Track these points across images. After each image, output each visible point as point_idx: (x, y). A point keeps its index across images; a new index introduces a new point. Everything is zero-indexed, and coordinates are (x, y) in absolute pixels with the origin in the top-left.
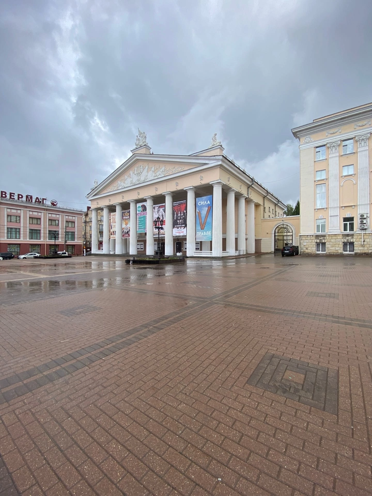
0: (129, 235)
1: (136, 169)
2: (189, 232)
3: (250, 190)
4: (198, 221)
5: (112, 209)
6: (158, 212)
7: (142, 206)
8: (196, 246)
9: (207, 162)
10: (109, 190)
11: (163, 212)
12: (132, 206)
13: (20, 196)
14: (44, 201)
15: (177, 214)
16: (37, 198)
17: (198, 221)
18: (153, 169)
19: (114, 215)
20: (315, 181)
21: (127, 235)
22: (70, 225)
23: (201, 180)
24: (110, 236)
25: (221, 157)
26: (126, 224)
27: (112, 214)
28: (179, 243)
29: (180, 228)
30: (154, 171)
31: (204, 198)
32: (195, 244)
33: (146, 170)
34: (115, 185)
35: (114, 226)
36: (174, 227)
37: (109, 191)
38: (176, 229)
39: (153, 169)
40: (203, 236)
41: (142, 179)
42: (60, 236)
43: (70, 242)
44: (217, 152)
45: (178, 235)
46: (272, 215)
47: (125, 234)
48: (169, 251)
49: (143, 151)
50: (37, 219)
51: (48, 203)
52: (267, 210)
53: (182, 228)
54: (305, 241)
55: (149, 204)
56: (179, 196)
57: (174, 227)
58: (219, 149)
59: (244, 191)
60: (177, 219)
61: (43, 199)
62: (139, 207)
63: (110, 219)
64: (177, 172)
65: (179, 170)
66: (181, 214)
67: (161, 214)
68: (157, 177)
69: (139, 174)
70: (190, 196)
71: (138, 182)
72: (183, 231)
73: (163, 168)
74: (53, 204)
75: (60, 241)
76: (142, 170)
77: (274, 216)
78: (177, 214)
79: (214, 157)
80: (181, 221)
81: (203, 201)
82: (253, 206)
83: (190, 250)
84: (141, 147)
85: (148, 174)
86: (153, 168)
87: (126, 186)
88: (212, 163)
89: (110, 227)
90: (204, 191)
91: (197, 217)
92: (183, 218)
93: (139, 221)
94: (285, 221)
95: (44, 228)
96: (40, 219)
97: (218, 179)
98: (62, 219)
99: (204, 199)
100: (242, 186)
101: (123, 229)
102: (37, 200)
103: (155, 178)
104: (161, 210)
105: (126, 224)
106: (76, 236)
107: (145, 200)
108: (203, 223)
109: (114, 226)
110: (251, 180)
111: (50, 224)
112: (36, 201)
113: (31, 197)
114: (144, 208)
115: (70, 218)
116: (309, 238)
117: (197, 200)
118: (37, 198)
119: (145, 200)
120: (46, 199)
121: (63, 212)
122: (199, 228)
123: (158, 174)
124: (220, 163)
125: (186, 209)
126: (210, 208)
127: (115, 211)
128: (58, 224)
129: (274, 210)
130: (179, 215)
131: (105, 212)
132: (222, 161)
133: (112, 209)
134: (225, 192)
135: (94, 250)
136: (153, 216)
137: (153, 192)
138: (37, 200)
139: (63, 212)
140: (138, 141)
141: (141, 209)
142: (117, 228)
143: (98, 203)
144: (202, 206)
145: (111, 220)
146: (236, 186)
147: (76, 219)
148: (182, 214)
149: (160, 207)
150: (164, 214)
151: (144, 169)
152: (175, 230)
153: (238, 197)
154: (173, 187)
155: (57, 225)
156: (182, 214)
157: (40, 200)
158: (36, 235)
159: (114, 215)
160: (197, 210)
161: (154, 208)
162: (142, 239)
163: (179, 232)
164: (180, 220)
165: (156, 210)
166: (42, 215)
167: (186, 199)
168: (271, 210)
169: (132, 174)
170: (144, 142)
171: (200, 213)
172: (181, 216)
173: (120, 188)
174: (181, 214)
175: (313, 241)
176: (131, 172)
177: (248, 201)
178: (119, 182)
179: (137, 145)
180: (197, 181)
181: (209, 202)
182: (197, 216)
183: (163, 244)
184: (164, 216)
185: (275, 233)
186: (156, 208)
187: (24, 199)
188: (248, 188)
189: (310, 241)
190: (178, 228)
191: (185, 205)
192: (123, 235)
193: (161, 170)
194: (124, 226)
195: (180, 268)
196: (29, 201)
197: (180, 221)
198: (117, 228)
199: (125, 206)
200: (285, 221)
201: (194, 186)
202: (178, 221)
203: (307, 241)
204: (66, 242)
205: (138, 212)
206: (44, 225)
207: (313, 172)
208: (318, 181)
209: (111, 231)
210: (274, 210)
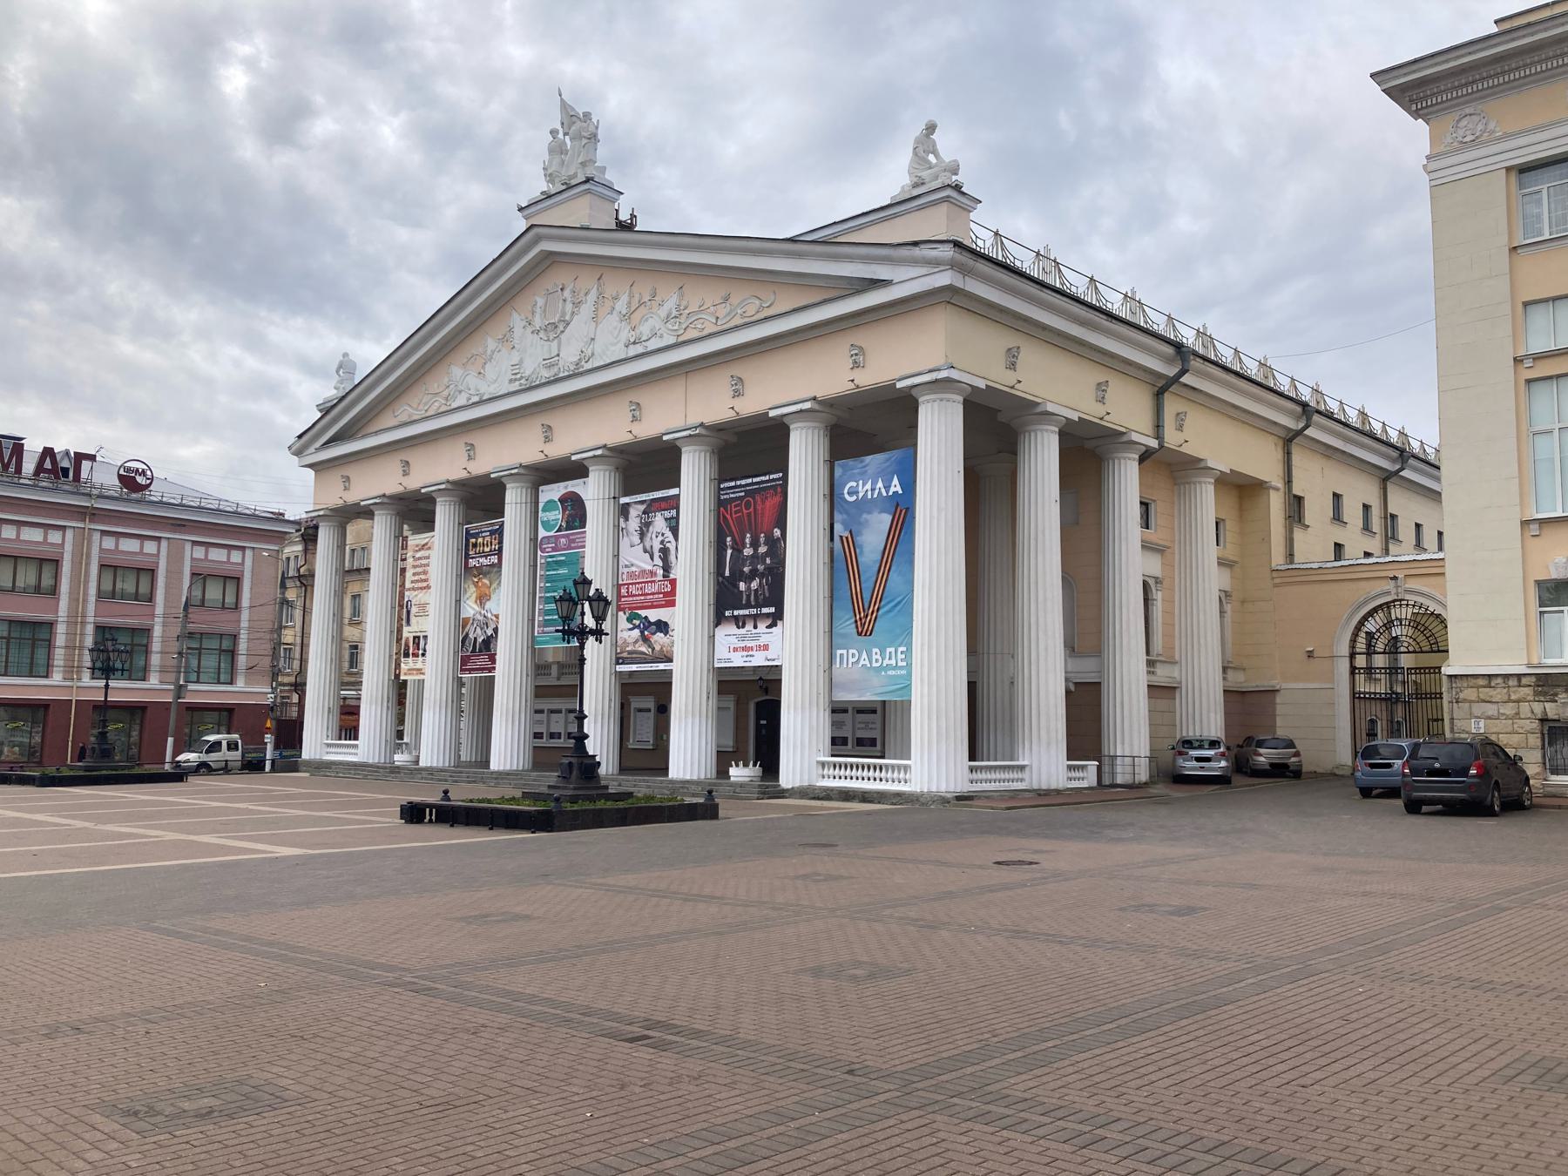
0: (493, 659)
1: (540, 301)
2: (790, 646)
3: (1171, 406)
4: (843, 592)
5: (414, 511)
6: (642, 535)
7: (563, 500)
8: (835, 724)
9: (881, 272)
10: (404, 411)
11: (669, 534)
12: (514, 498)
14: (86, 465)
15: (738, 549)
17: (843, 592)
18: (621, 305)
19: (423, 547)
20: (1518, 361)
21: (483, 660)
22: (214, 592)
23: (856, 365)
24: (398, 666)
25: (947, 252)
26: (482, 599)
27: (415, 540)
28: (752, 705)
29: (749, 626)
30: (626, 317)
31: (874, 461)
32: (828, 713)
33: (587, 309)
34: (434, 387)
35: (423, 606)
36: (719, 619)
37: (404, 418)
38: (732, 629)
39: (621, 305)
40: (865, 670)
41: (569, 356)
42: (155, 660)
43: (203, 692)
44: (933, 224)
45: (738, 661)
46: (1356, 544)
47: (476, 651)
48: (689, 752)
49: (577, 212)
50: (42, 561)
52: (1317, 510)
53: (762, 626)
54: (1478, 709)
55: (595, 490)
56: (751, 449)
57: (719, 619)
58: (944, 207)
59: (1127, 411)
60: (737, 575)
61: (80, 457)
62: (550, 505)
63: (403, 570)
64: (738, 321)
65: (751, 309)
66: (755, 544)
67: (657, 547)
68: (639, 349)
69: (555, 329)
70: (804, 454)
71: (546, 374)
72: (763, 640)
73: (671, 304)
75: (153, 687)
76: (569, 307)
77: (1374, 545)
78: (738, 549)
79: (917, 252)
80: (754, 585)
81: (867, 482)
82: (1206, 502)
83: (803, 751)
84: (571, 187)
85: (599, 330)
86: (624, 298)
87: (488, 390)
88: (908, 281)
89: (402, 611)
90: (870, 427)
91: (840, 564)
92: (769, 569)
93: (548, 579)
94: (1412, 584)
95: (74, 612)
97: (939, 361)
98: (174, 564)
99: (871, 470)
101: (466, 621)
102: (48, 465)
103: (633, 351)
104: (659, 522)
105: (482, 599)
106: (242, 661)
107: (577, 470)
108: (865, 597)
109: (423, 606)
110: (1170, 350)
111: (107, 586)
112: (39, 469)
114: (575, 511)
115: (217, 555)
116: (1498, 694)
117: (838, 472)
118: (48, 452)
119: (577, 470)
120: (92, 458)
121: (180, 525)
122: (847, 626)
123: (645, 330)
124: (944, 279)
125: (783, 526)
126: (902, 512)
127: (425, 522)
129: (1376, 513)
130: (748, 551)
131: (380, 530)
132: (953, 265)
133: (414, 511)
134: (994, 429)
135: (316, 741)
136: (617, 556)
137: (612, 427)
138: (48, 465)
139: (180, 525)
140: (557, 160)
141: (557, 516)
142: (432, 622)
144: (864, 505)
145: (409, 574)
146: (1061, 388)
147: (245, 561)
148: (763, 549)
149: (652, 507)
150: (672, 546)
151: (577, 304)
152: (727, 636)
153: (1086, 453)
154: (713, 403)
156: (763, 549)
157: (65, 464)
158: (27, 651)
159: (423, 547)
160: (838, 528)
161: (624, 511)
162: (556, 686)
163: (738, 648)
164: (754, 574)
165: (634, 524)
166: (64, 541)
167: (784, 469)
168: (1352, 513)
169: (518, 331)
170: (583, 164)
171: (851, 543)
172: (755, 556)
173: (461, 401)
174: (755, 544)
175: (1525, 707)
176: (517, 320)
177: (1170, 468)
178: (456, 371)
179: (550, 178)
180: (829, 375)
181: (896, 487)
182: (841, 560)
183: (770, 712)
184: (672, 558)
185: (1352, 656)
186: (634, 512)
188: (1159, 394)
189: (1508, 709)
190: (740, 622)
191: (778, 499)
192: (465, 660)
193: (663, 312)
194: (470, 609)
197: (747, 589)
198: (432, 622)
199: (482, 499)
200: (1412, 584)
201: (820, 394)
202: (742, 586)
203: (1491, 710)
204: (180, 690)
205: (542, 533)
206: (74, 600)
207: (1507, 308)
208: (1538, 357)
209: (407, 633)
210: (1376, 513)
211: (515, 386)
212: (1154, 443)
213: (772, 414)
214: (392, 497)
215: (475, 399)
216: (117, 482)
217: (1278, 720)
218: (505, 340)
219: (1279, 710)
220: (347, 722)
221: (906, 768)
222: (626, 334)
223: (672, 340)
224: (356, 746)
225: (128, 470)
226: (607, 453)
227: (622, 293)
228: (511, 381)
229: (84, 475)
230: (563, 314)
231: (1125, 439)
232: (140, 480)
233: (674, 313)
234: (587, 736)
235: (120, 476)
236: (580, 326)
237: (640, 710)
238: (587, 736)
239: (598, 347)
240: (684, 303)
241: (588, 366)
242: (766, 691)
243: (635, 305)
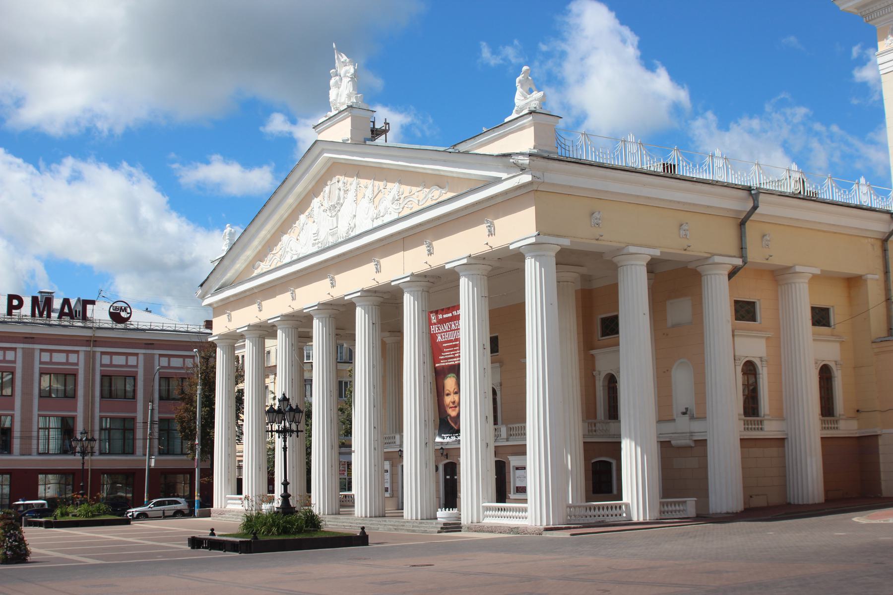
13: (15, 302)
14: (89, 307)
16: (66, 302)
33: (351, 195)
39: (369, 193)
51: (100, 313)
61: (85, 303)
69: (335, 208)
73: (394, 192)
74: (115, 316)
96: (75, 375)
100: (447, 392)
102: (66, 310)
103: (379, 222)
113: (49, 301)
123: (382, 208)
128: (134, 391)
138: (66, 310)
143: (213, 534)
151: (346, 191)
155: (130, 395)
169: (316, 210)
173: (287, 260)
187: (26, 309)
193: (390, 197)
195: (747, 506)
196: (41, 315)
211: (315, 249)
212: (738, 262)
213: (448, 266)
214: (368, 291)
215: (295, 258)
216: (109, 318)
217: (881, 456)
218: (310, 216)
219: (881, 449)
220: (504, 487)
221: (525, 510)
222: (373, 212)
223: (395, 216)
224: (525, 510)
225: (116, 309)
226: (365, 294)
227: (368, 186)
228: (314, 245)
229: (89, 314)
230: (339, 199)
231: (710, 261)
232: (123, 314)
233: (397, 197)
234: (290, 496)
235: (111, 314)
236: (347, 208)
237: (517, 469)
238: (290, 496)
239: (357, 221)
240: (401, 190)
241: (353, 234)
242: (447, 456)
243: (376, 191)
